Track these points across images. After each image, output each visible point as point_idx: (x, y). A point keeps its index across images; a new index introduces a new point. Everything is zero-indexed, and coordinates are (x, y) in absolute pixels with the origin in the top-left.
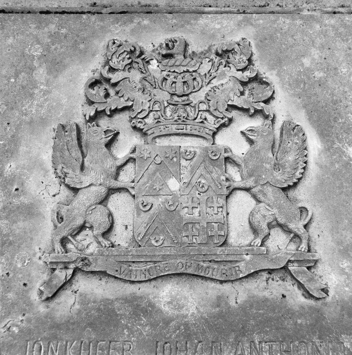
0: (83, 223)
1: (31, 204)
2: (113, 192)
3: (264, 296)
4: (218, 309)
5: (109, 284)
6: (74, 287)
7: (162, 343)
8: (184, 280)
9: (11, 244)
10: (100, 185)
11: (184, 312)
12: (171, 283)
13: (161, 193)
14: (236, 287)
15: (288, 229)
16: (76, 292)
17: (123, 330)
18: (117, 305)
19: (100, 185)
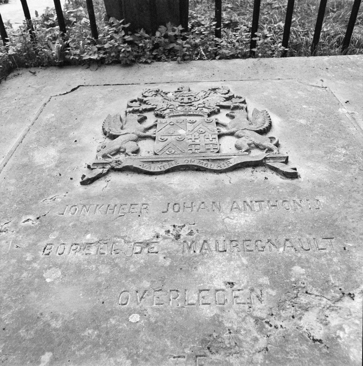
0: (119, 147)
1: (84, 147)
2: (140, 139)
3: (260, 130)
4: (216, 186)
5: (133, 177)
6: (107, 179)
7: (173, 204)
8: (189, 173)
9: (66, 162)
10: (133, 133)
11: (190, 188)
12: (180, 175)
13: (173, 134)
14: (229, 175)
15: (263, 146)
16: (108, 181)
17: (142, 198)
18: (138, 186)
19: (133, 133)
